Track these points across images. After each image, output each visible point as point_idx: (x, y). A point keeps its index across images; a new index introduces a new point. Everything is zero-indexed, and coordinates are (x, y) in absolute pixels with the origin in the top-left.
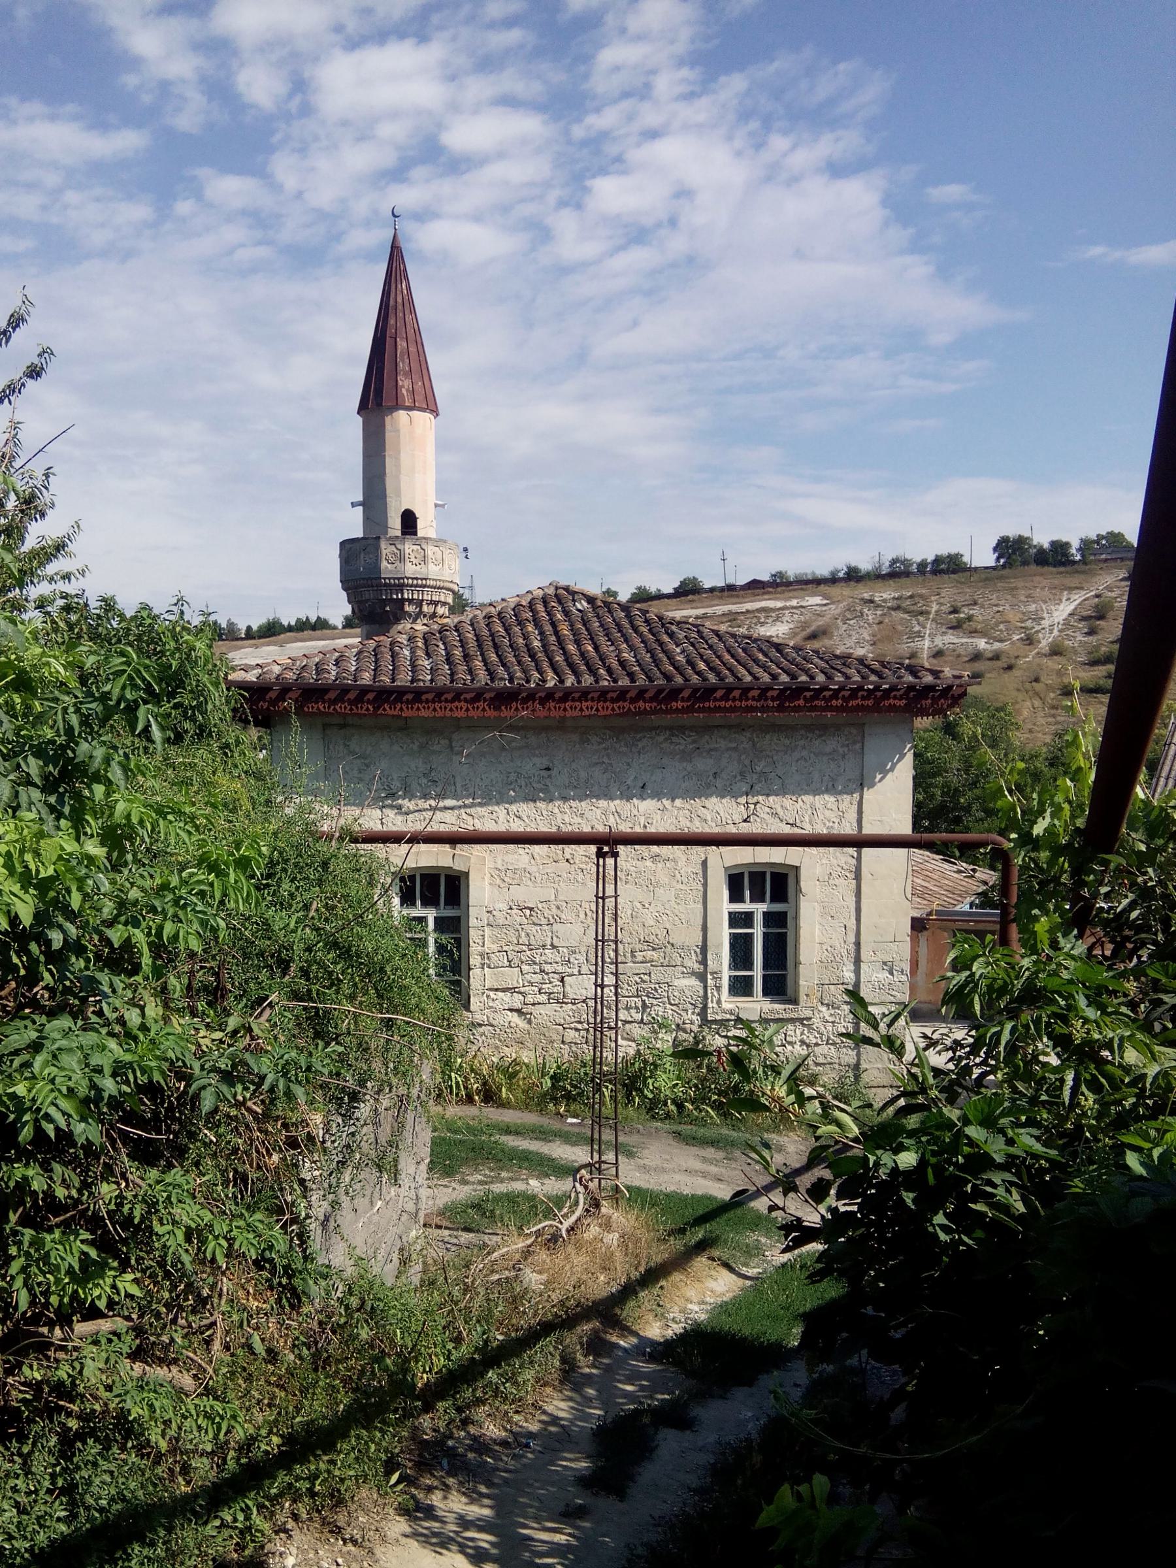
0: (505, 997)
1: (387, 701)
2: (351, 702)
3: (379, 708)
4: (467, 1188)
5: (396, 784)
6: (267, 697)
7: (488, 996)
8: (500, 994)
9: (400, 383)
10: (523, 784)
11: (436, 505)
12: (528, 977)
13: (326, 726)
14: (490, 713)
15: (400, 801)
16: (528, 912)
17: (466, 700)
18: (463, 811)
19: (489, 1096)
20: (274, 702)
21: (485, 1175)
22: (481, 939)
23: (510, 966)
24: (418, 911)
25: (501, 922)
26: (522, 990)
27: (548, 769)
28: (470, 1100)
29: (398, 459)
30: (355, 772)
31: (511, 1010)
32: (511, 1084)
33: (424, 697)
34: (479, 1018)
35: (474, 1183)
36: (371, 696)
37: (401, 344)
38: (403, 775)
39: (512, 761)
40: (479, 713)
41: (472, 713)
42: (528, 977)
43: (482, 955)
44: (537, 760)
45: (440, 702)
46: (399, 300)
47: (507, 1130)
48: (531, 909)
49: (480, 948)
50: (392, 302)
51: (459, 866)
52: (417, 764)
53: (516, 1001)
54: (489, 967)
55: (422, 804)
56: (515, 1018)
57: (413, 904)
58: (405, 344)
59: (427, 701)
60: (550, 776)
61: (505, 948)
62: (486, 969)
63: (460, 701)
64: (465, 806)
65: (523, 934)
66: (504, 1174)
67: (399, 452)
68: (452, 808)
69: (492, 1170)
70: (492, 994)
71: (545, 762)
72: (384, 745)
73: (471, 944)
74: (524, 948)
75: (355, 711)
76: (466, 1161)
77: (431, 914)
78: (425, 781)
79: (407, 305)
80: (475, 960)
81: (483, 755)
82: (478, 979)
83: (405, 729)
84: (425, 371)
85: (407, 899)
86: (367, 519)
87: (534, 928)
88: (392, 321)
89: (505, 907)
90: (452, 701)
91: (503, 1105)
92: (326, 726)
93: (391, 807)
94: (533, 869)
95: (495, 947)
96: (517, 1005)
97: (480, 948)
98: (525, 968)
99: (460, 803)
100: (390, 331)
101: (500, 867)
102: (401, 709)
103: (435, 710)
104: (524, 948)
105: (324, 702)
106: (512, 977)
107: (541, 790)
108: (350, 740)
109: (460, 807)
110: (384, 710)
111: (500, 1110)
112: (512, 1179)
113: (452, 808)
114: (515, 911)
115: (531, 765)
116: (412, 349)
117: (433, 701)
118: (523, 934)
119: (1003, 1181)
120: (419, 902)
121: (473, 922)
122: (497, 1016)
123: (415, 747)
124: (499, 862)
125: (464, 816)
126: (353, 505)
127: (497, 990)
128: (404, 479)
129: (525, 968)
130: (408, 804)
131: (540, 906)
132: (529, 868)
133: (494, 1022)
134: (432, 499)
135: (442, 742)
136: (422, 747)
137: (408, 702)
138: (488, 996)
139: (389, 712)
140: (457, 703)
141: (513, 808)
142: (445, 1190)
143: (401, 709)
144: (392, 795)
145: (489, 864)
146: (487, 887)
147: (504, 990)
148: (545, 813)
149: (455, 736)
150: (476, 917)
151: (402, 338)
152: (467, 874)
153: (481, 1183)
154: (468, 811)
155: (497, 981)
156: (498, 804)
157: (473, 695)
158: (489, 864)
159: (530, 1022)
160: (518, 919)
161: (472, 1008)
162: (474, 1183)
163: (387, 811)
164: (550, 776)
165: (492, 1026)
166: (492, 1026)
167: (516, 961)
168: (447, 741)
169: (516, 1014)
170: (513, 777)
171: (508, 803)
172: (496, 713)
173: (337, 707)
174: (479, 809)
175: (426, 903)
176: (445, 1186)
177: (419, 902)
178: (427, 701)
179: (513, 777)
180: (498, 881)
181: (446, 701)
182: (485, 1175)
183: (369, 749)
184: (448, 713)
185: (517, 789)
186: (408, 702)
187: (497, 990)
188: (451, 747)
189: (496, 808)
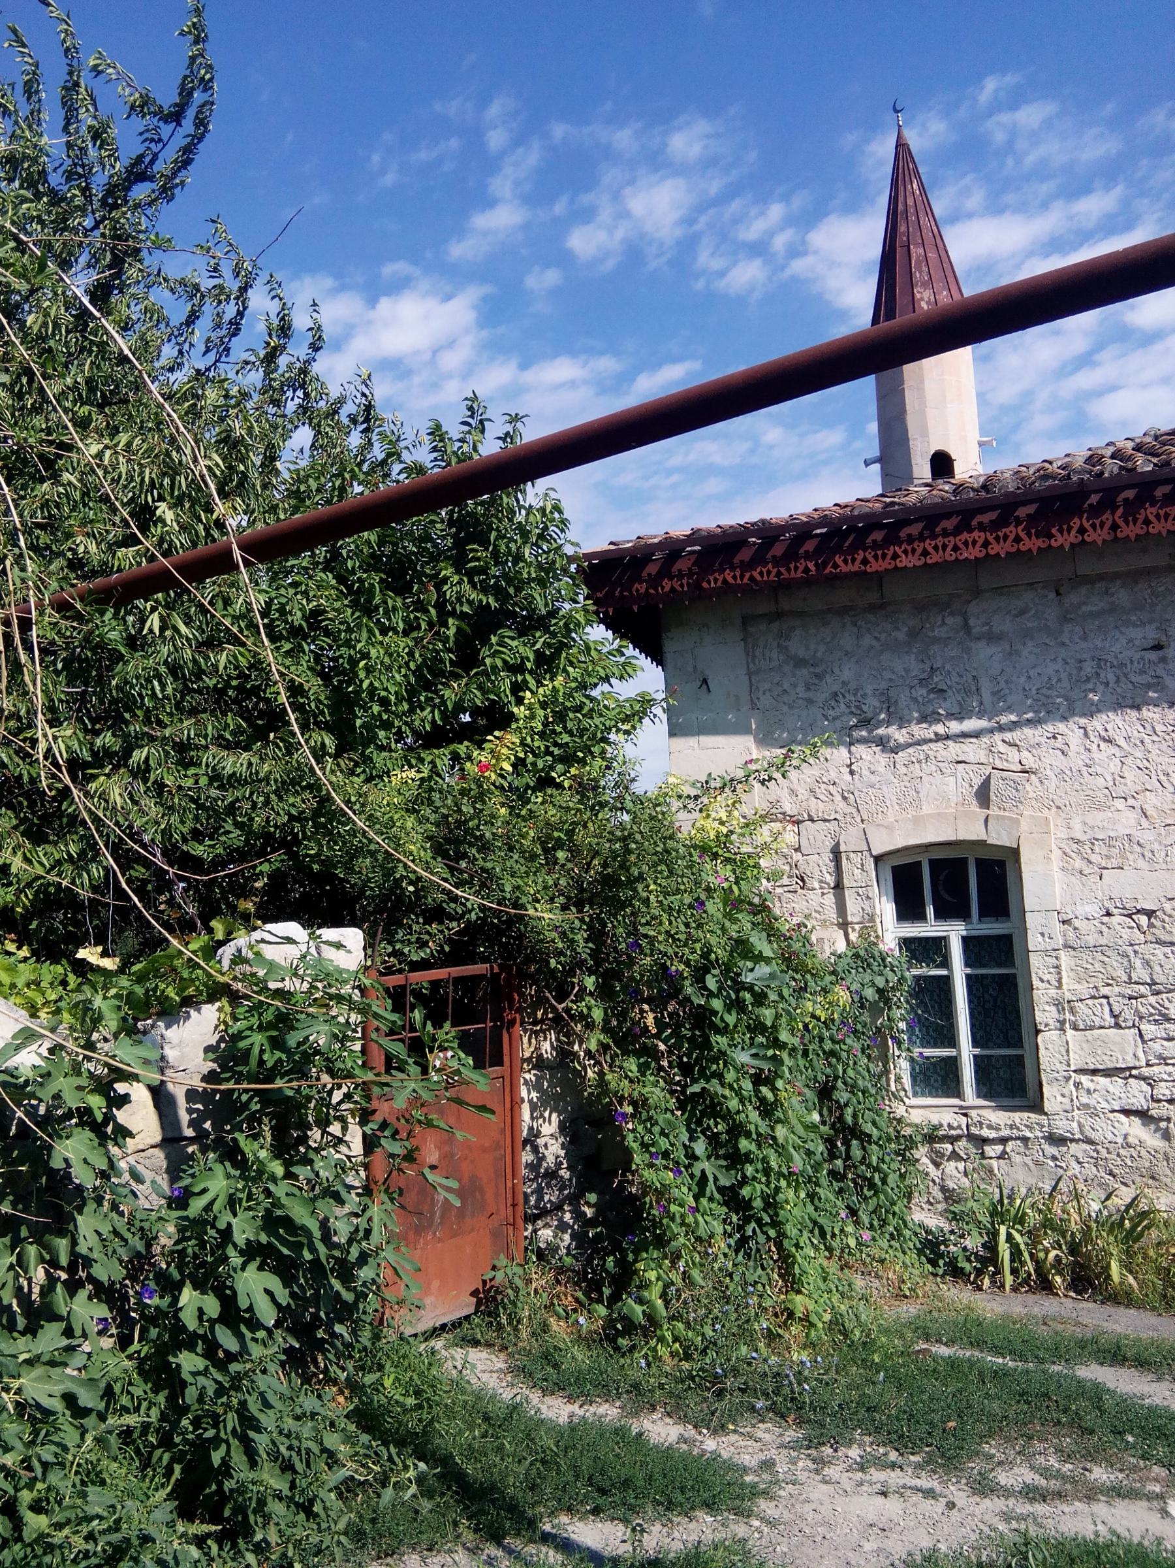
0: (1114, 1085)
1: (838, 549)
2: (776, 562)
3: (825, 564)
4: (990, 1506)
5: (872, 703)
6: (644, 574)
7: (1078, 1085)
8: (1102, 1081)
9: (918, 296)
10: (1111, 678)
11: (980, 444)
12: (1157, 1047)
13: (746, 620)
14: (1031, 544)
15: (881, 731)
16: (1143, 920)
17: (982, 527)
18: (998, 737)
19: (1086, 1279)
20: (654, 581)
21: (1045, 1472)
22: (1053, 976)
23: (1117, 1026)
24: (930, 928)
25: (1091, 940)
26: (1146, 1071)
27: (1158, 647)
28: (1045, 1286)
29: (921, 390)
30: (800, 689)
31: (1127, 1112)
32: (1129, 1252)
33: (903, 534)
34: (1062, 1126)
35: (1008, 1493)
36: (810, 546)
37: (916, 252)
38: (884, 685)
39: (1085, 638)
40: (1008, 547)
41: (995, 548)
42: (1157, 1047)
43: (1058, 1004)
44: (1136, 633)
45: (934, 537)
46: (910, 202)
47: (1115, 1354)
48: (1150, 914)
49: (1053, 992)
50: (901, 207)
51: (999, 837)
52: (907, 664)
53: (1137, 1094)
54: (1075, 1028)
55: (920, 731)
56: (1135, 1129)
57: (920, 916)
58: (921, 251)
59: (910, 539)
60: (1163, 660)
61: (1105, 991)
62: (1070, 1032)
63: (971, 531)
64: (1001, 728)
65: (1138, 963)
66: (1100, 1474)
67: (922, 381)
68: (976, 735)
69: (1066, 1456)
70: (1085, 1079)
71: (1151, 634)
72: (847, 640)
73: (1036, 983)
74: (1143, 989)
75: (786, 575)
76: (996, 1427)
77: (954, 933)
78: (924, 692)
79: (921, 207)
80: (1045, 1014)
81: (1027, 634)
82: (1055, 1051)
83: (882, 606)
84: (951, 280)
85: (908, 909)
86: (886, 475)
87: (1160, 951)
88: (902, 228)
89: (1095, 910)
90: (957, 531)
91: (1119, 1298)
92: (746, 620)
93: (864, 741)
94: (1147, 836)
95: (1084, 990)
96: (1140, 1102)
97: (1053, 992)
98: (1149, 1029)
99: (993, 724)
100: (901, 240)
101: (1079, 835)
102: (865, 562)
103: (925, 553)
104: (1143, 989)
105: (733, 569)
106: (1122, 1047)
107: (1149, 686)
108: (788, 638)
109: (991, 731)
110: (836, 566)
111: (1109, 1309)
112: (1117, 1492)
113: (976, 735)
114: (1116, 919)
115: (1125, 643)
116: (932, 255)
117: (922, 538)
118: (1138, 963)
119: (153, 1182)
120: (930, 911)
121: (1034, 941)
122: (1099, 1123)
123: (901, 635)
124: (1077, 825)
125: (1002, 748)
126: (867, 463)
127: (1094, 1072)
128: (931, 413)
129: (1149, 1029)
130: (898, 735)
131: (1168, 906)
132: (1138, 835)
133: (1093, 1135)
134: (974, 436)
135: (950, 621)
136: (913, 634)
137: (875, 545)
138: (1078, 1085)
139: (844, 568)
140: (964, 536)
141: (1097, 724)
142: (927, 1505)
143: (865, 562)
144: (866, 722)
145: (1058, 832)
146: (1058, 876)
147: (1109, 1073)
148: (1160, 728)
149: (973, 608)
150: (1040, 932)
151: (916, 244)
152: (1015, 853)
153: (1032, 1494)
154: (1008, 736)
155: (1094, 1053)
156: (1064, 718)
157: (993, 515)
158: (1058, 832)
159: (1167, 1136)
160: (1125, 933)
161: (1047, 1106)
162: (1008, 1493)
163: (860, 750)
164: (1163, 660)
165: (1091, 1142)
166: (1091, 1142)
167: (1128, 1015)
168: (958, 620)
169: (1136, 1121)
170: (1089, 668)
171: (1084, 715)
172: (1040, 543)
173: (756, 574)
174: (1028, 731)
175: (941, 915)
176: (929, 1494)
177: (930, 911)
178: (910, 539)
179: (1089, 668)
180: (1079, 864)
181: (946, 533)
182: (1045, 1472)
183: (822, 648)
184: (950, 555)
185: (1101, 688)
186: (875, 545)
187: (1094, 1072)
188: (967, 627)
189: (1061, 727)
